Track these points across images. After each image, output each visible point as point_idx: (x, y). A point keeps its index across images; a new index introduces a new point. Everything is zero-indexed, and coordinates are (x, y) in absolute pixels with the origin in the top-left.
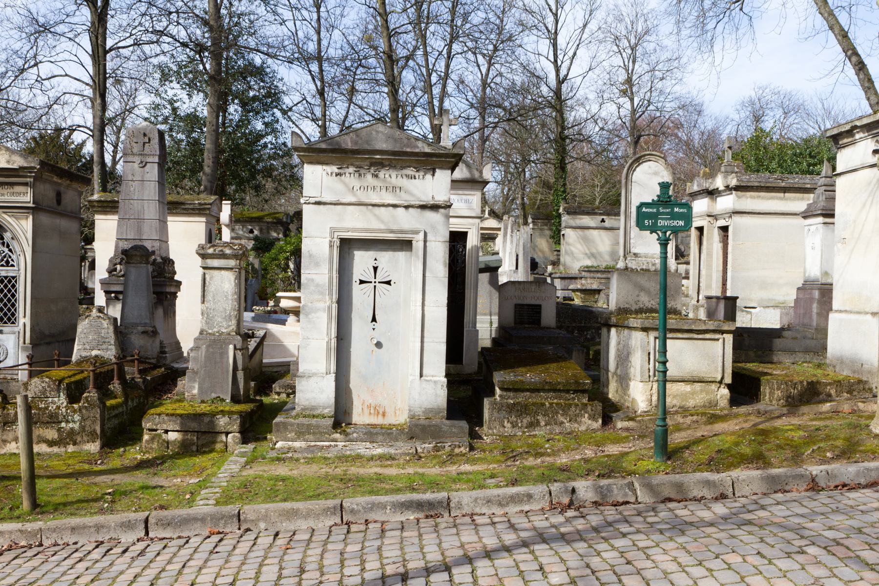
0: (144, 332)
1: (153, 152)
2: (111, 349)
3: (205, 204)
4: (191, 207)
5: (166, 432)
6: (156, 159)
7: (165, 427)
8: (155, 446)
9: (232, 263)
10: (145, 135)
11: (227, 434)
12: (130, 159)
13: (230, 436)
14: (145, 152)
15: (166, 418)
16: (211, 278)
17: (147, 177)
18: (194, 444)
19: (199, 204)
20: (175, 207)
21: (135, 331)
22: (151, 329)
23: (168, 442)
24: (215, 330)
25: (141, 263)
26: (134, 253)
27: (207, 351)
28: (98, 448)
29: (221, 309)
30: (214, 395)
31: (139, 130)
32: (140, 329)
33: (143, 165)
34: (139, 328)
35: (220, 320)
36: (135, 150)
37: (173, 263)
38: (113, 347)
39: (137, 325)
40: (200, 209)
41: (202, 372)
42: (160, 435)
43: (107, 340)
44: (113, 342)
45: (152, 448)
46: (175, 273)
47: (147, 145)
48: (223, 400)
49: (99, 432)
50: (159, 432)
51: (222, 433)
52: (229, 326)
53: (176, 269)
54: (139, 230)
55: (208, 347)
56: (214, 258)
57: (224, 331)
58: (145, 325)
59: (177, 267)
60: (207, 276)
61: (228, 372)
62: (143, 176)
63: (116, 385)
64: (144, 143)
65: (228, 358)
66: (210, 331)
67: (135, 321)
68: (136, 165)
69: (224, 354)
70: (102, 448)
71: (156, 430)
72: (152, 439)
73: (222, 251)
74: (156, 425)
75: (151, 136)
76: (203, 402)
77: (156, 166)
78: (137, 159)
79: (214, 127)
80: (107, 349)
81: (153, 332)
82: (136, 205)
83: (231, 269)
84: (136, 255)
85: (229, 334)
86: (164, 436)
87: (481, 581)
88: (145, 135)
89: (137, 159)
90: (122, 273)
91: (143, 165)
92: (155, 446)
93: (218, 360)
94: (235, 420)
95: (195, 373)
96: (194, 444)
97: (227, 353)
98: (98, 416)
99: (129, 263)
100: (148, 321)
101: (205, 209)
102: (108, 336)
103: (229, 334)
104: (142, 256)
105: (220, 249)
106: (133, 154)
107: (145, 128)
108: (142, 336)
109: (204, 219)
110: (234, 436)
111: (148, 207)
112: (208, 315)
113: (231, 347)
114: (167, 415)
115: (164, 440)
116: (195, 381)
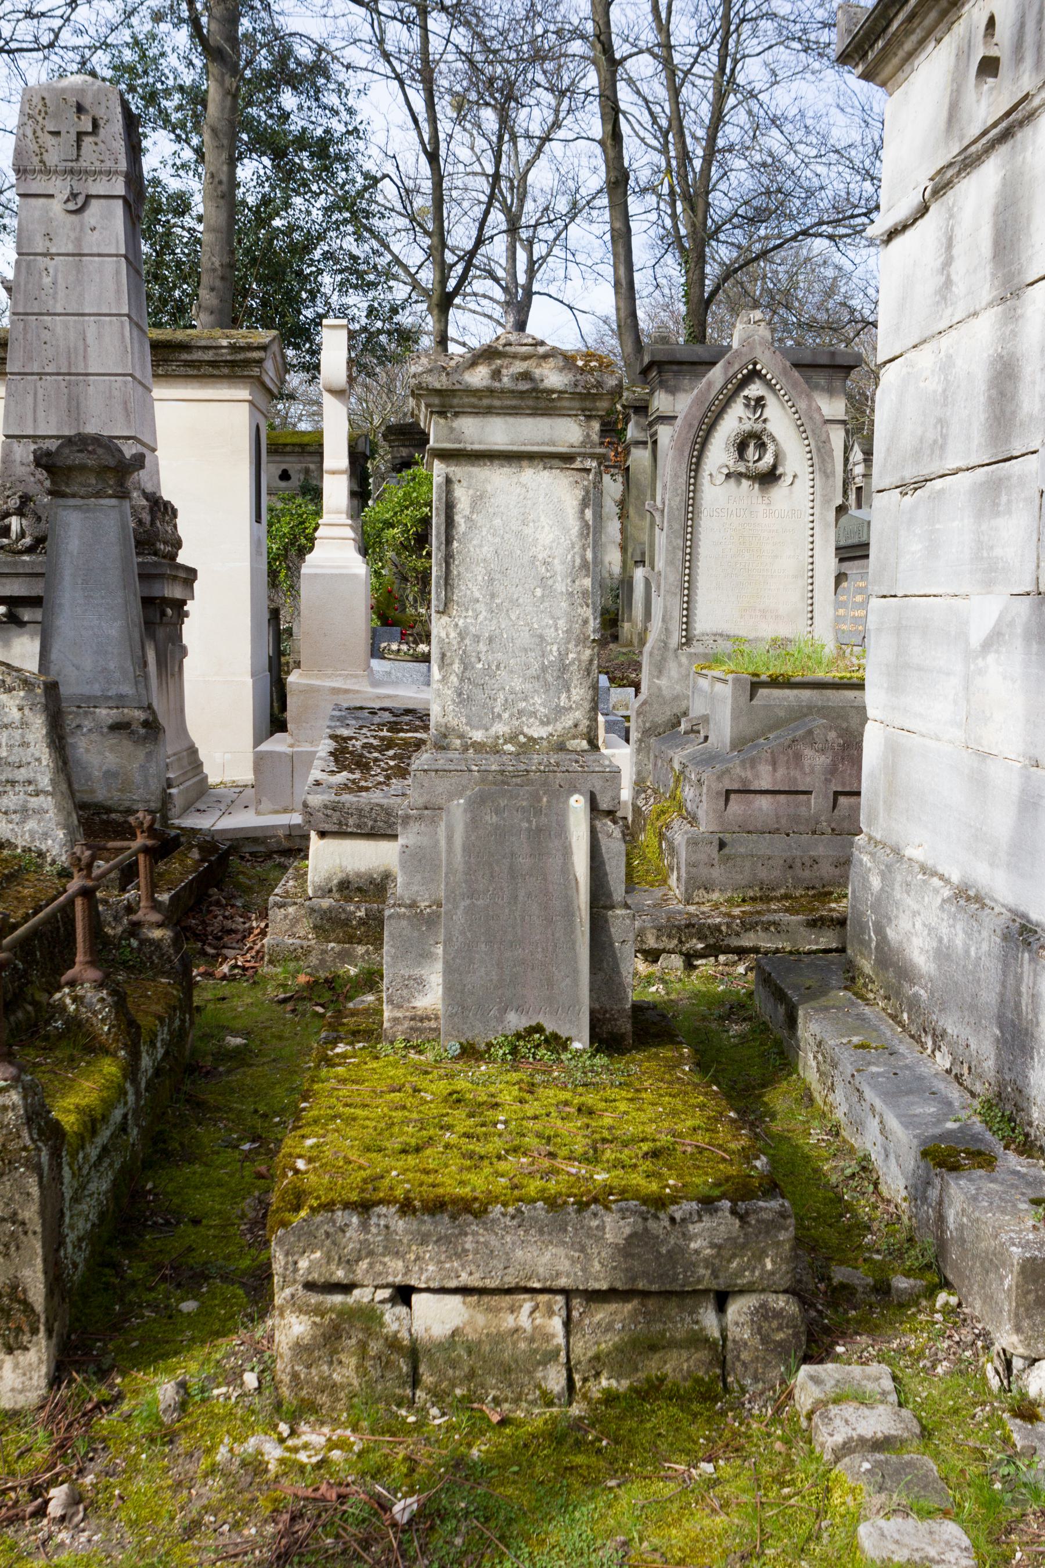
0: (117, 727)
1: (109, 164)
2: (40, 812)
3: (250, 348)
4: (209, 356)
5: (403, 1294)
6: (119, 187)
7: (396, 1271)
8: (346, 1372)
9: (568, 432)
10: (80, 109)
11: (721, 1300)
12: (37, 185)
13: (737, 1309)
14: (83, 164)
15: (400, 1225)
16: (478, 500)
17: (92, 243)
18: (552, 1356)
19: (233, 348)
20: (171, 360)
21: (87, 724)
22: (140, 715)
23: (414, 1353)
24: (500, 728)
25: (98, 495)
26: (79, 458)
27: (474, 823)
28: (39, 1378)
29: (525, 638)
30: (516, 1022)
31: (62, 96)
32: (105, 714)
33: (79, 204)
34: (102, 712)
35: (517, 684)
36: (52, 159)
37: (174, 513)
38: (47, 802)
39: (93, 702)
40: (232, 364)
41: (459, 916)
42: (369, 1316)
43: (22, 774)
44: (45, 781)
45: (330, 1388)
46: (178, 544)
47: (88, 140)
48: (557, 1043)
49: (37, 1293)
50: (361, 1296)
51: (697, 1294)
52: (560, 711)
53: (182, 531)
54: (74, 408)
55: (477, 803)
56: (489, 411)
57: (538, 731)
58: (120, 701)
59: (184, 527)
60: (461, 493)
61: (569, 913)
62: (78, 241)
63: (88, 992)
64: (80, 135)
65: (567, 852)
66: (478, 736)
67: (86, 690)
68: (56, 206)
69: (548, 833)
70: (54, 1381)
71: (346, 1288)
72: (329, 1339)
73: (526, 376)
74: (350, 1264)
75: (101, 113)
76: (469, 1052)
77: (118, 206)
78: (60, 187)
79: (224, 188)
80: (24, 812)
81: (146, 724)
82: (59, 330)
83: (566, 458)
84: (83, 468)
85: (561, 747)
86: (393, 1318)
87: (5, 733)
88: (80, 109)
89: (60, 187)
90: (28, 541)
91: (79, 204)
92: (346, 1372)
93: (524, 862)
94: (771, 1226)
95: (426, 921)
96: (552, 1356)
97: (562, 830)
98: (30, 1213)
99: (63, 495)
100: (127, 689)
101: (247, 363)
102: (27, 755)
103: (561, 747)
104: (103, 471)
105: (519, 367)
106: (47, 171)
107: (82, 91)
108: (113, 740)
109: (244, 394)
110: (763, 1313)
111: (99, 337)
112: (466, 666)
113: (578, 803)
114: (406, 1207)
115: (393, 1343)
116: (425, 956)
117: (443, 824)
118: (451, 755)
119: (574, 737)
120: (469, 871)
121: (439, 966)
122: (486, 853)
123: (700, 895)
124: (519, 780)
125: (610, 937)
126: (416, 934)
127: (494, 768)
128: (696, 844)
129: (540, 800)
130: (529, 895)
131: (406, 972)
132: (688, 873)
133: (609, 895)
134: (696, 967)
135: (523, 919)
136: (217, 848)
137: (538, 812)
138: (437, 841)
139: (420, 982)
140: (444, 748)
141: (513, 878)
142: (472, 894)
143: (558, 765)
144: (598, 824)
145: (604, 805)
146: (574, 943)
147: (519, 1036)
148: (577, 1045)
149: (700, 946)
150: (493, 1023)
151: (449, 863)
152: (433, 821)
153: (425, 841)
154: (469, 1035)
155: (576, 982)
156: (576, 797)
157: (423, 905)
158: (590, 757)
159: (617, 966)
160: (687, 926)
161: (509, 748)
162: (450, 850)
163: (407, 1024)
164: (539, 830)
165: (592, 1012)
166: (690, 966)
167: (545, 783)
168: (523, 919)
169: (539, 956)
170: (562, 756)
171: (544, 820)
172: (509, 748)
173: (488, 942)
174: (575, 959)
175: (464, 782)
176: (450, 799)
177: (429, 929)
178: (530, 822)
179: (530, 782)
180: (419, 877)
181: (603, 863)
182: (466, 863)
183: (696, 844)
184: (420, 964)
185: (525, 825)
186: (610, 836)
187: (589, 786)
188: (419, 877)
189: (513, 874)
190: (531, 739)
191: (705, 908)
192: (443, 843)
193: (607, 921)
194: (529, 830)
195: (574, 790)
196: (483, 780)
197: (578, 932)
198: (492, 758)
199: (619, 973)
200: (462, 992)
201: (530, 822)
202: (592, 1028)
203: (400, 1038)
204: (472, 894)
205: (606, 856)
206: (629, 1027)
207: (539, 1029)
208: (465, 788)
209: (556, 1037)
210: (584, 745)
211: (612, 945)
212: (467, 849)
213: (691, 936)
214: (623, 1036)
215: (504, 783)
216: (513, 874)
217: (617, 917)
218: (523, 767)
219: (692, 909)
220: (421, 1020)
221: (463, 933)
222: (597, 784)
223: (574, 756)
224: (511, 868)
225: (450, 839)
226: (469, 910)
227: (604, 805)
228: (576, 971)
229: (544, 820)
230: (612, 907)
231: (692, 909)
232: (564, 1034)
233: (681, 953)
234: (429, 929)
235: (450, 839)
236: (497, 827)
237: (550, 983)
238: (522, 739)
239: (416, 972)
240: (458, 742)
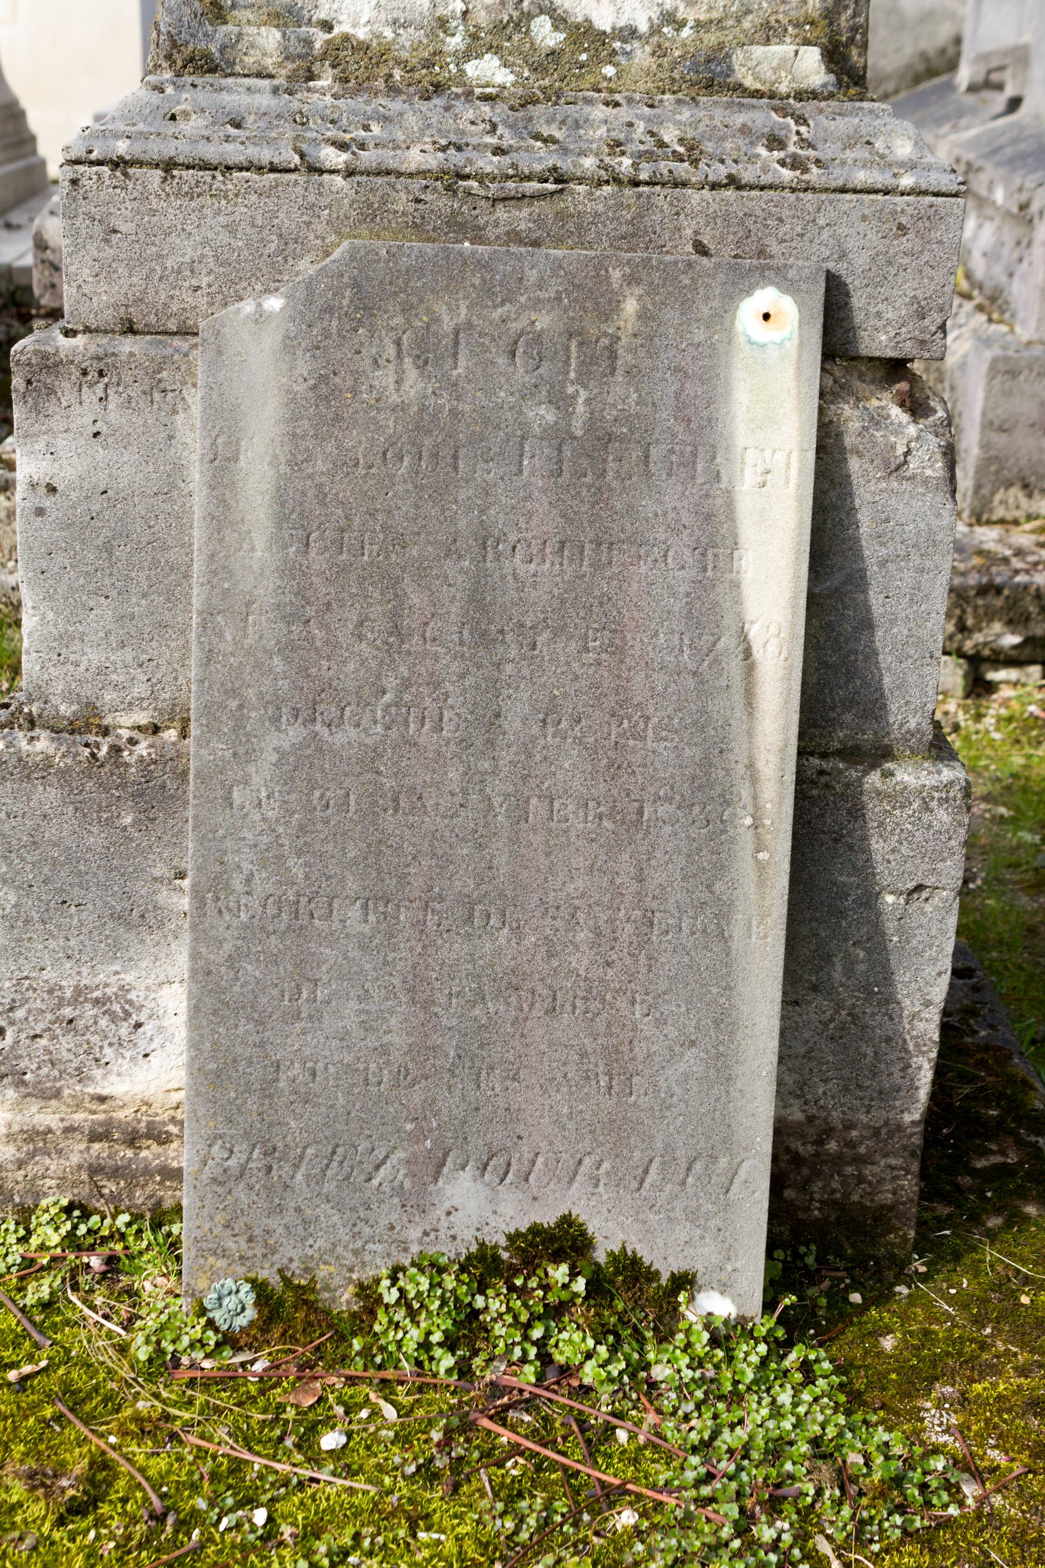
27: (325, 400)
30: (478, 1211)
48: (635, 1298)
55: (346, 313)
61: (709, 789)
65: (713, 537)
69: (635, 453)
93: (533, 575)
97: (697, 442)
103: (710, 77)
113: (770, 334)
116: (133, 920)
117: (194, 398)
118: (238, 95)
119: (769, 33)
120: (302, 604)
121: (181, 961)
122: (371, 533)
123: (1010, 501)
124: (522, 217)
125: (865, 870)
126: (96, 838)
127: (415, 158)
128: (1013, 373)
129: (609, 310)
130: (548, 715)
131: (66, 977)
132: (985, 446)
133: (874, 707)
134: (991, 688)
135: (520, 813)
136: (895, 106)
137: (601, 359)
138: (178, 468)
139: (124, 1013)
140: (207, 65)
141: (484, 639)
142: (313, 704)
143: (692, 152)
144: (851, 417)
145: (877, 340)
146: (724, 912)
147: (484, 1267)
148: (716, 1304)
149: (1011, 640)
150: (388, 1213)
151: (219, 569)
152: (158, 387)
153: (126, 468)
154: (291, 1255)
155: (722, 1067)
156: (766, 297)
157: (125, 722)
158: (833, 124)
159: (887, 978)
160: (983, 590)
161: (489, 70)
162: (222, 515)
163: (77, 1152)
164: (602, 439)
165: (781, 1130)
166: (978, 687)
167: (635, 235)
168: (520, 813)
169: (580, 961)
170: (713, 113)
171: (621, 394)
172: (489, 70)
173: (378, 899)
174: (724, 976)
175: (288, 219)
176: (227, 294)
177: (146, 819)
178: (561, 401)
179: (571, 229)
180: (104, 614)
181: (859, 580)
182: (289, 570)
183: (1013, 373)
184: (116, 950)
185: (546, 415)
186: (897, 469)
187: (813, 257)
188: (104, 614)
189: (484, 624)
190: (584, 34)
191: (1022, 538)
192: (196, 475)
193: (857, 812)
194: (558, 437)
195: (755, 265)
196: (370, 214)
197: (744, 867)
198: (413, 113)
199: (887, 1002)
200: (267, 1092)
201: (561, 401)
202: (778, 1183)
203: (54, 1200)
204: (313, 704)
205: (872, 552)
206: (909, 1185)
207: (566, 1241)
208: (291, 245)
209: (631, 1269)
210: (811, 66)
211: (870, 900)
212: (295, 517)
213: (990, 615)
214: (882, 1217)
215: (460, 227)
216: (484, 624)
217: (900, 798)
218: (542, 158)
219: (988, 536)
220: (132, 1140)
221: (272, 859)
222: (853, 239)
223: (763, 117)
224: (478, 600)
225: (222, 464)
226: (300, 769)
227: (877, 340)
228: (724, 1021)
229: (621, 394)
230: (881, 754)
231: (988, 536)
232: (665, 1263)
233: (960, 654)
234: (146, 819)
235: (222, 464)
236: (423, 421)
237: (618, 1066)
238: (545, 33)
239: (106, 977)
240: (270, 38)
